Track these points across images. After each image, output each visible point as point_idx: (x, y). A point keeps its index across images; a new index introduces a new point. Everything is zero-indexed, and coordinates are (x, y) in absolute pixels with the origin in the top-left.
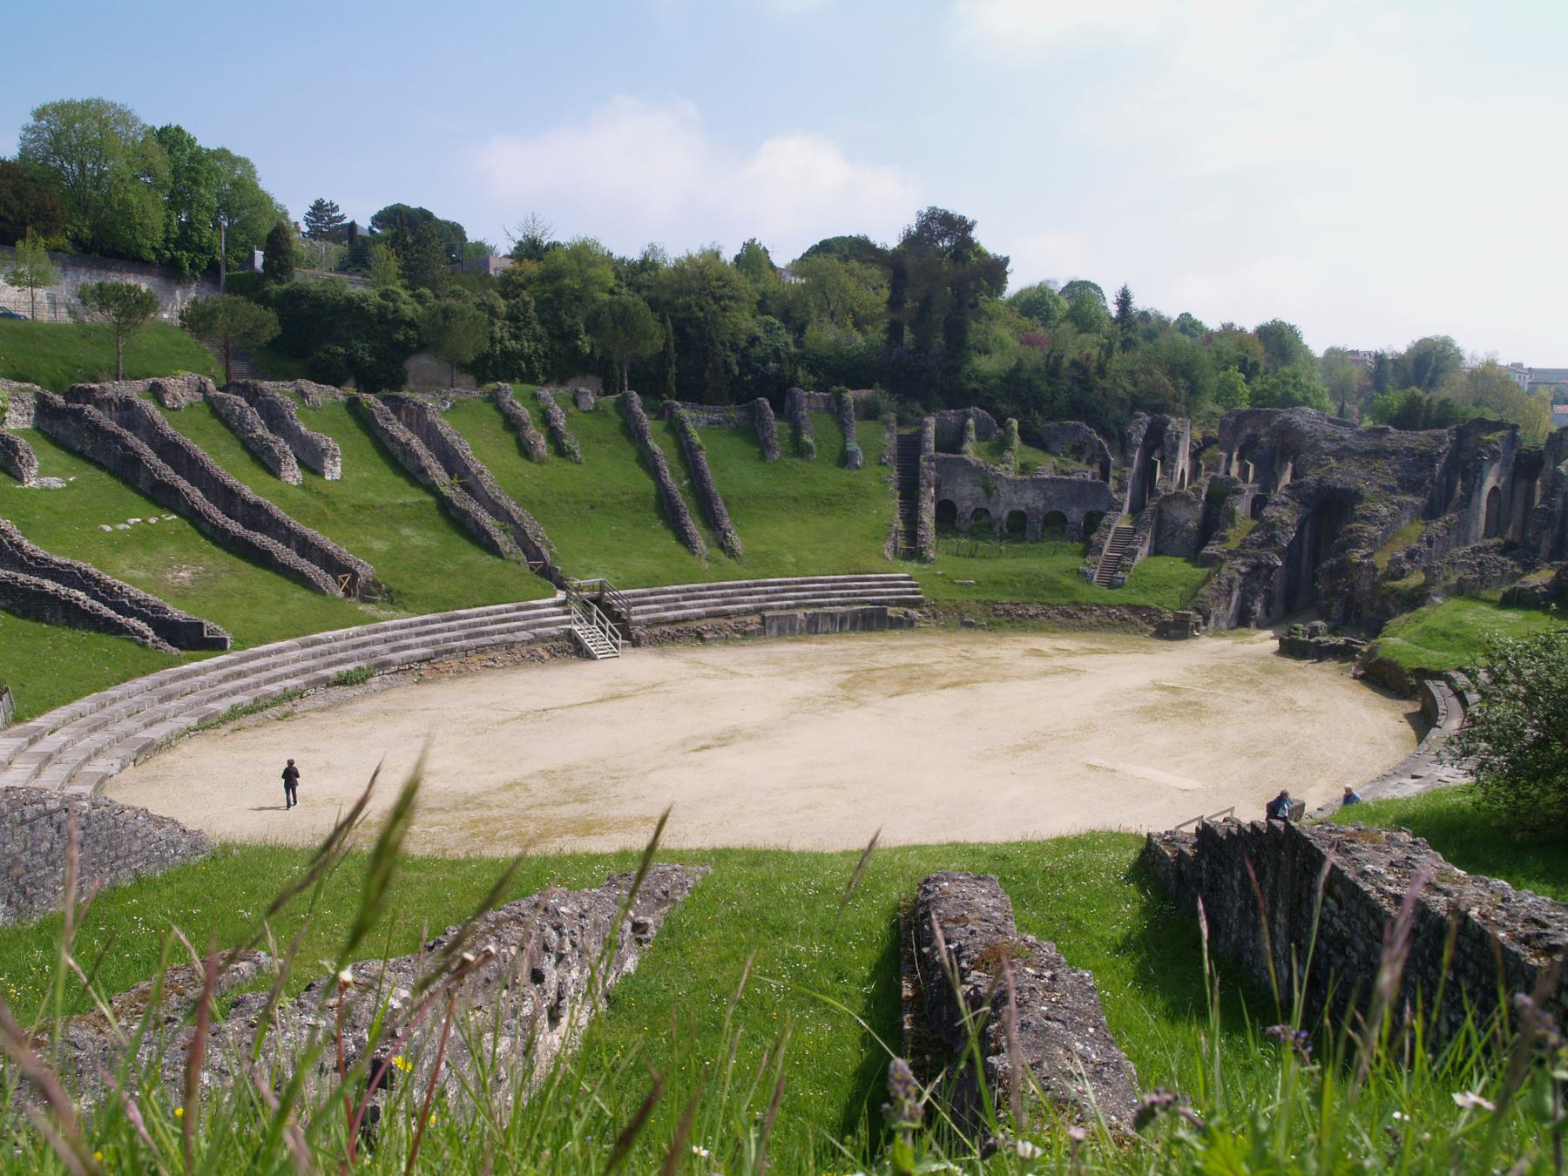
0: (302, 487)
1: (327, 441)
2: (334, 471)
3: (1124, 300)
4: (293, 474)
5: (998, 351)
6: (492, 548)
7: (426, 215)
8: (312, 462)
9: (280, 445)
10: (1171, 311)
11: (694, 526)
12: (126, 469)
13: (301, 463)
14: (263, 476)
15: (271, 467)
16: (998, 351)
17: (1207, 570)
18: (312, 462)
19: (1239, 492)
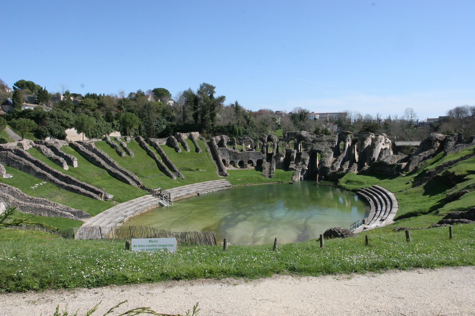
0: (69, 170)
1: (72, 157)
2: (76, 164)
3: (104, 94)
4: (66, 167)
5: (221, 119)
6: (127, 182)
7: (33, 83)
8: (70, 162)
9: (61, 159)
10: (255, 109)
11: (170, 172)
12: (27, 169)
13: (68, 164)
14: (59, 167)
15: (61, 165)
16: (221, 119)
17: (451, 171)
18: (70, 162)
19: (293, 152)
